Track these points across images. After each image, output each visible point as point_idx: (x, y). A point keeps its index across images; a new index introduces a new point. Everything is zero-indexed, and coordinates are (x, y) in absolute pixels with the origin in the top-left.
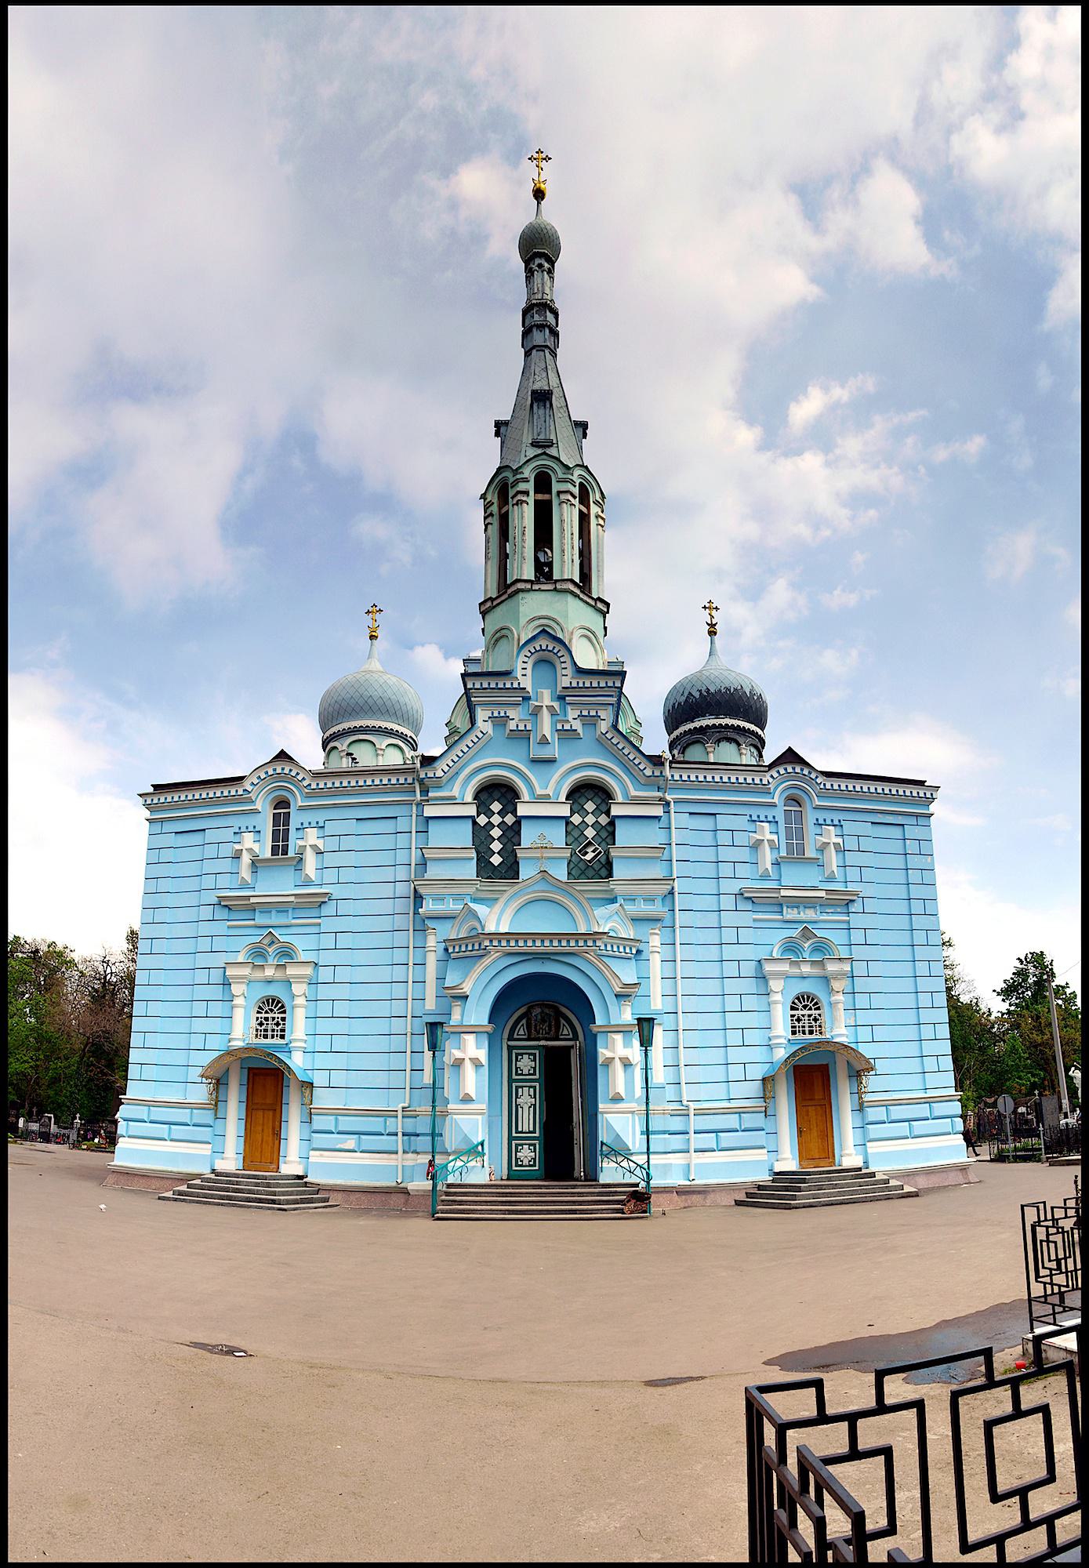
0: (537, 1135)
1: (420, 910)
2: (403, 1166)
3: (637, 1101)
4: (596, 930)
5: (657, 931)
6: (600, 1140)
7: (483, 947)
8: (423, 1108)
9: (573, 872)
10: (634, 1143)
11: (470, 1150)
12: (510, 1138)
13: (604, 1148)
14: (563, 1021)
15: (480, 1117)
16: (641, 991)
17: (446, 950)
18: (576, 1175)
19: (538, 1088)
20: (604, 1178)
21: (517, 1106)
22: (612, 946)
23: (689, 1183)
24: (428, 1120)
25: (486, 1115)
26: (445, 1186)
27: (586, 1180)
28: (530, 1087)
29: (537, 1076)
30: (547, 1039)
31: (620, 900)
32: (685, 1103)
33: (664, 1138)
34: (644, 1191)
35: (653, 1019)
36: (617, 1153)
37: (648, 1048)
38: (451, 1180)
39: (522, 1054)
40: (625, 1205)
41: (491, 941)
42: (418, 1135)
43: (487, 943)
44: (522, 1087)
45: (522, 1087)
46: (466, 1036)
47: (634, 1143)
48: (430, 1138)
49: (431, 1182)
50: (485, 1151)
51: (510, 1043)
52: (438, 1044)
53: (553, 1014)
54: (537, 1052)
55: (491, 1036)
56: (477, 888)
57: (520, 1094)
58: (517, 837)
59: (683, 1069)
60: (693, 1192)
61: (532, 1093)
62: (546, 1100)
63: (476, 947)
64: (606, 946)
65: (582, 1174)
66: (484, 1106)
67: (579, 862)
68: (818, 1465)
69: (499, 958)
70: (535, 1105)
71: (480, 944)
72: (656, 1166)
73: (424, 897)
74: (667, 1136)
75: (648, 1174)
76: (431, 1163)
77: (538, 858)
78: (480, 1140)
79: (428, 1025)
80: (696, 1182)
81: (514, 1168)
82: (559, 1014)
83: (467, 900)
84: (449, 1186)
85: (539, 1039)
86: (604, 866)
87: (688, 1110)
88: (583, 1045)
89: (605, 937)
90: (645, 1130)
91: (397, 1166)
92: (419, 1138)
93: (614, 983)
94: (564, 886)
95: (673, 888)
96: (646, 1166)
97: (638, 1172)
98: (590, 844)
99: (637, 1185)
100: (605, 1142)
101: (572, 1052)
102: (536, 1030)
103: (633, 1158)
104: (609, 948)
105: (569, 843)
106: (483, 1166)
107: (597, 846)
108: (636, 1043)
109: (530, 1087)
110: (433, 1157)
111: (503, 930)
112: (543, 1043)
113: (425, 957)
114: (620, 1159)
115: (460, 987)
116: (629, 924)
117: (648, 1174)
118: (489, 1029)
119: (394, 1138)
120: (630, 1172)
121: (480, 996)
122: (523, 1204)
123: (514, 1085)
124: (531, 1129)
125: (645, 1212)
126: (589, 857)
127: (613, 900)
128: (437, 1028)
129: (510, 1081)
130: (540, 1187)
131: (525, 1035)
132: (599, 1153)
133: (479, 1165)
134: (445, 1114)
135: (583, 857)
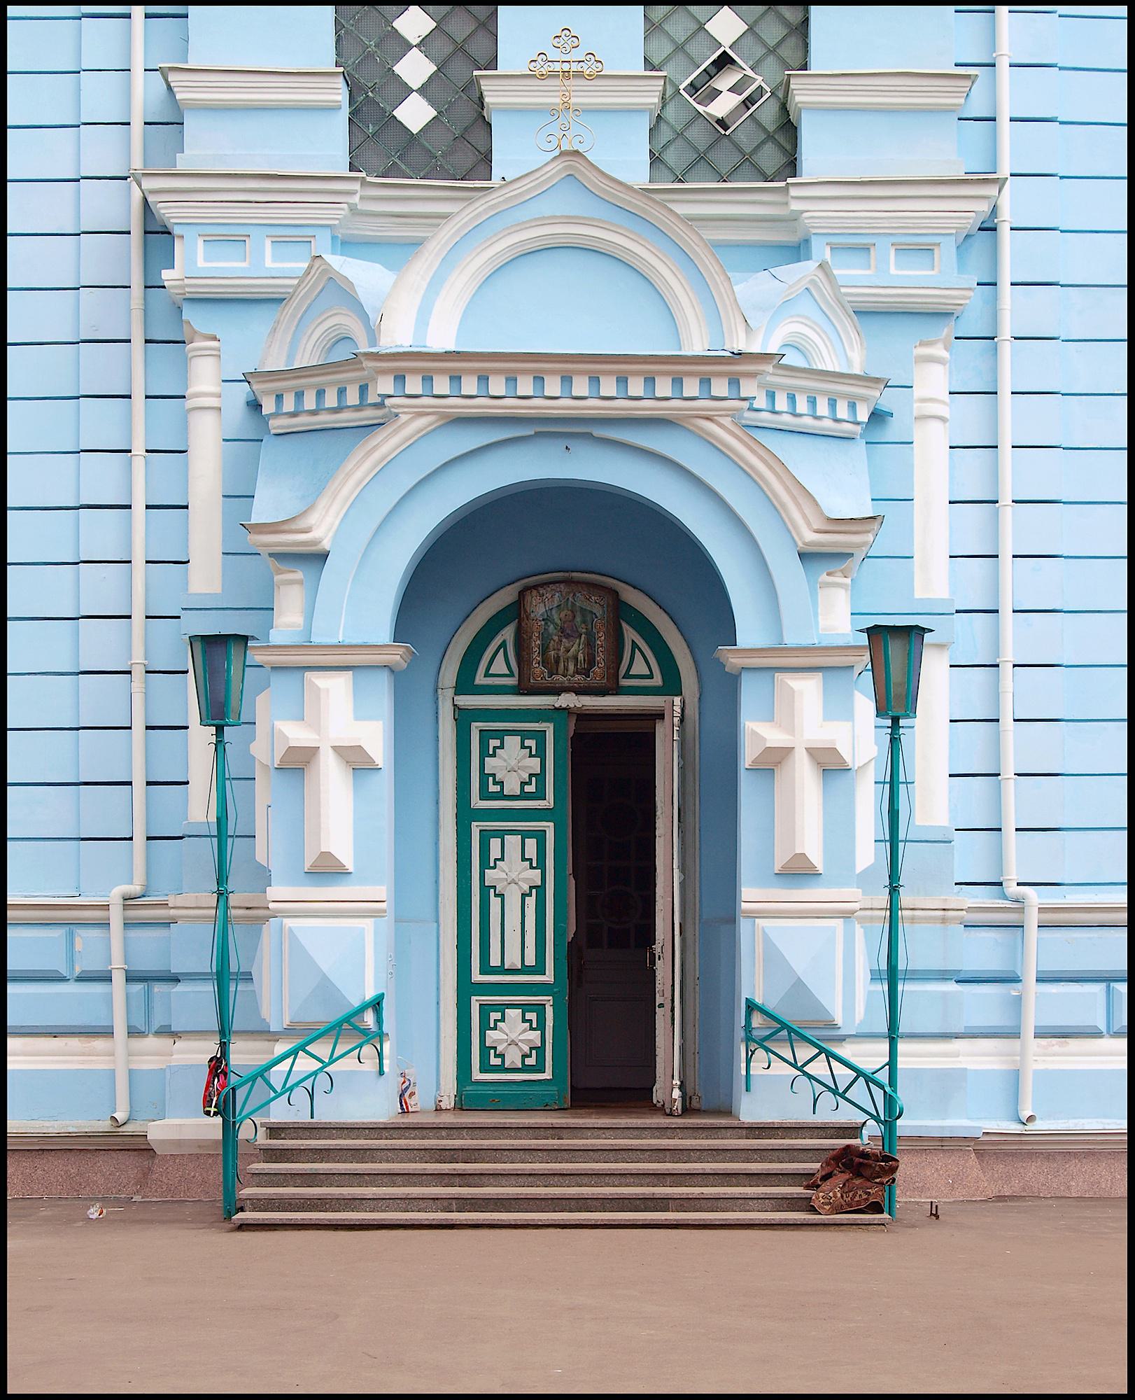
0: (549, 977)
1: (166, 274)
2: (131, 1072)
3: (864, 879)
4: (741, 345)
5: (939, 351)
6: (745, 994)
7: (372, 398)
8: (188, 899)
9: (670, 157)
10: (849, 1006)
11: (339, 1024)
12: (466, 988)
13: (757, 1020)
14: (630, 634)
15: (368, 924)
16: (883, 542)
17: (255, 406)
18: (658, 1095)
19: (549, 1012)
20: (751, 1110)
21: (485, 890)
22: (792, 399)
23: (1015, 1128)
24: (206, 933)
25: (389, 918)
26: (261, 1131)
27: (687, 1110)
28: (525, 834)
29: (549, 802)
30: (579, 691)
31: (821, 251)
32: (1012, 889)
33: (945, 995)
34: (876, 1147)
35: (924, 630)
36: (795, 1035)
37: (902, 723)
38: (280, 1113)
39: (501, 734)
40: (815, 1186)
41: (400, 379)
42: (175, 979)
43: (385, 385)
44: (501, 834)
45: (501, 834)
46: (321, 681)
47: (849, 1006)
48: (209, 988)
49: (219, 1120)
50: (385, 1029)
51: (466, 701)
52: (233, 702)
53: (598, 611)
54: (549, 728)
55: (401, 680)
56: (353, 209)
57: (495, 852)
58: (482, 41)
59: (1011, 785)
60: (1031, 1155)
61: (531, 850)
62: (575, 874)
63: (352, 398)
64: (771, 396)
65: (676, 1093)
66: (381, 891)
67: (689, 124)
68: (871, 1075)
69: (426, 435)
70: (540, 889)
71: (363, 390)
72: (916, 1073)
73: (177, 231)
74: (951, 987)
75: (890, 1101)
76: (218, 1067)
77: (552, 111)
78: (370, 994)
79: (198, 646)
80: (1039, 1126)
81: (477, 1075)
82: (620, 611)
83: (322, 245)
84: (275, 1131)
85: (557, 691)
86: (770, 137)
87: (1021, 910)
88: (692, 711)
89: (770, 368)
90: (884, 966)
91: (112, 1073)
92: (180, 988)
93: (796, 516)
94: (639, 202)
95: (994, 211)
96: (883, 1077)
97: (859, 1092)
98: (724, 62)
99: (855, 1131)
100: (758, 1000)
101: (661, 731)
102: (545, 663)
103: (844, 1051)
104: (782, 403)
105: (656, 61)
106: (381, 1073)
107: (750, 73)
108: (865, 705)
109: (525, 834)
110: (223, 1046)
111: (441, 338)
112: (567, 700)
113: (185, 428)
114: (804, 1052)
115: (301, 524)
116: (847, 326)
117: (890, 1101)
118: (396, 657)
119: (98, 988)
120: (835, 1092)
121: (364, 555)
122: (503, 1180)
123: (476, 828)
124: (531, 960)
125: (877, 1208)
126: (723, 106)
127: (798, 250)
128: (227, 656)
129: (465, 815)
130: (556, 1131)
131: (511, 675)
132: (739, 1034)
133: (370, 1066)
134: (259, 916)
135: (700, 108)
